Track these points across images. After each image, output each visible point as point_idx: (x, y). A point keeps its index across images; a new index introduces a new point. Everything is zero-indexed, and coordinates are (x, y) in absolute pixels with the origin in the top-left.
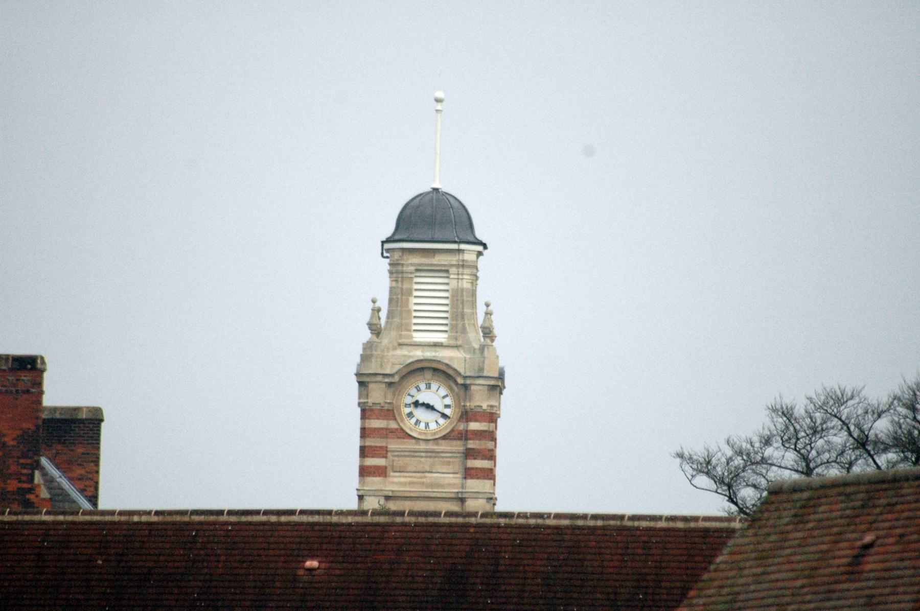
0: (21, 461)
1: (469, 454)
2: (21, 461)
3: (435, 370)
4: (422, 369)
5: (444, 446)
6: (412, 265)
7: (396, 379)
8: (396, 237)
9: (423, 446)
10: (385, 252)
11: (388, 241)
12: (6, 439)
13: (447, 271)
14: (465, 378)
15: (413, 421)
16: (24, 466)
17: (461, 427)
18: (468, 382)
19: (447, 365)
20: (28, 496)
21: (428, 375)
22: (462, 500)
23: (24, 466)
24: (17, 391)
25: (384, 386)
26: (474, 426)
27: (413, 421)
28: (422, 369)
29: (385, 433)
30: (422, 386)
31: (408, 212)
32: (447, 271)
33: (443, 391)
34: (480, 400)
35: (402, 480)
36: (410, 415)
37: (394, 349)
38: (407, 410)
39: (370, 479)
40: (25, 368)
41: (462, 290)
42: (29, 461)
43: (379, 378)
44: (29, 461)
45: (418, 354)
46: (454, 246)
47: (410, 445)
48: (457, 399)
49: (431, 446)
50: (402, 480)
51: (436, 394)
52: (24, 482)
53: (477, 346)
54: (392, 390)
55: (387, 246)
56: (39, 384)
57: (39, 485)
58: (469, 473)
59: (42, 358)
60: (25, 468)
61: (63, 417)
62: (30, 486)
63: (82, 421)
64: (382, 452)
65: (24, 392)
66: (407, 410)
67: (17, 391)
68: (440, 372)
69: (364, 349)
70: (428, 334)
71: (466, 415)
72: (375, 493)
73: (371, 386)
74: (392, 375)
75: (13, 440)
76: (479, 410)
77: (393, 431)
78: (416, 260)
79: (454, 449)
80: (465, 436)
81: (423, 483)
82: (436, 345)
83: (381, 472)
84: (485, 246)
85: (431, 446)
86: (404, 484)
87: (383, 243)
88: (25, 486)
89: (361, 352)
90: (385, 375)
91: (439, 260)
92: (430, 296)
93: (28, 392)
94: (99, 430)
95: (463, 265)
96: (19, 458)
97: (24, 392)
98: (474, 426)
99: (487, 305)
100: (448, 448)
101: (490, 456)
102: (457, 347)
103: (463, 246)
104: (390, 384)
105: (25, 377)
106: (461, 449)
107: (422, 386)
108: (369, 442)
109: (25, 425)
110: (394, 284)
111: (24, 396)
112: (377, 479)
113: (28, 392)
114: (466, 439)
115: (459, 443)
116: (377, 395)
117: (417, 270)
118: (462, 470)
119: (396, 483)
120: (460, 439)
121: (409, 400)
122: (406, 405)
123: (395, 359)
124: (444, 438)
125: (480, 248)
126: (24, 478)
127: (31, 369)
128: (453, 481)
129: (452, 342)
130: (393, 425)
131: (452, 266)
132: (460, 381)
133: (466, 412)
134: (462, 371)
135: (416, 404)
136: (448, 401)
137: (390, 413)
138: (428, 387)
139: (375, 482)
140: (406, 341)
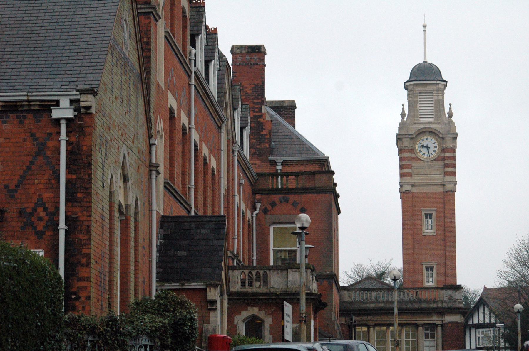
0: (255, 101)
1: (446, 166)
2: (255, 101)
3: (430, 132)
4: (425, 132)
5: (435, 163)
6: (418, 91)
7: (414, 136)
8: (411, 80)
9: (426, 164)
10: (406, 88)
11: (407, 82)
12: (246, 90)
13: (432, 93)
14: (443, 134)
15: (422, 154)
16: (256, 104)
17: (442, 155)
18: (444, 136)
19: (435, 129)
20: (259, 120)
21: (427, 134)
22: (444, 185)
23: (256, 104)
24: (251, 64)
25: (409, 139)
26: (447, 154)
27: (422, 154)
28: (425, 132)
29: (411, 159)
30: (425, 139)
31: (415, 70)
32: (432, 93)
33: (434, 141)
34: (449, 143)
35: (418, 178)
36: (420, 151)
37: (412, 125)
38: (419, 149)
39: (405, 178)
40: (255, 52)
41: (439, 100)
42: (259, 101)
43: (407, 136)
44: (259, 101)
45: (422, 126)
46: (435, 82)
47: (421, 163)
48: (440, 144)
49: (430, 164)
50: (418, 178)
51: (431, 142)
52: (257, 112)
53: (446, 122)
54: (412, 141)
55: (406, 84)
56: (263, 60)
57: (265, 113)
58: (446, 174)
59: (263, 46)
60: (256, 105)
61: (276, 105)
62: (260, 114)
63: (286, 107)
64: (410, 167)
65: (254, 64)
66: (419, 149)
67: (251, 64)
68: (432, 133)
69: (400, 129)
70: (426, 120)
71: (444, 150)
72: (408, 184)
73: (404, 140)
74: (412, 135)
75: (250, 90)
76: (449, 147)
77: (414, 158)
78: (420, 88)
79: (440, 165)
80: (444, 159)
81: (427, 179)
82: (429, 123)
83: (410, 175)
84: (447, 82)
85: (430, 164)
86: (419, 180)
87: (405, 83)
88: (257, 114)
89: (397, 131)
90: (410, 135)
91: (429, 88)
92: (426, 103)
93: (257, 64)
94: (294, 111)
95: (439, 90)
96: (253, 99)
97: (254, 64)
98: (447, 154)
99: (450, 105)
100: (437, 164)
101: (454, 166)
102: (438, 123)
103: (438, 82)
104: (411, 139)
105: (255, 56)
106: (443, 164)
107: (425, 139)
108: (404, 163)
109: (256, 82)
110: (410, 99)
111: (255, 66)
112: (408, 178)
113: (257, 64)
114: (445, 160)
115: (441, 162)
116: (406, 143)
117: (420, 93)
118: (443, 173)
119: (416, 179)
120: (442, 160)
121: (420, 145)
122: (419, 147)
123: (414, 128)
124: (435, 160)
125: (445, 83)
126: (256, 110)
127: (258, 52)
128: (439, 178)
129: (437, 122)
130: (413, 156)
131: (434, 90)
132: (441, 136)
133: (444, 149)
134: (441, 132)
135: (423, 146)
136: (436, 145)
137: (412, 150)
138: (427, 139)
139: (407, 179)
140: (417, 122)
